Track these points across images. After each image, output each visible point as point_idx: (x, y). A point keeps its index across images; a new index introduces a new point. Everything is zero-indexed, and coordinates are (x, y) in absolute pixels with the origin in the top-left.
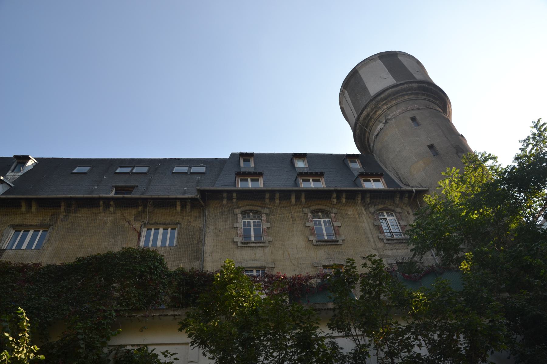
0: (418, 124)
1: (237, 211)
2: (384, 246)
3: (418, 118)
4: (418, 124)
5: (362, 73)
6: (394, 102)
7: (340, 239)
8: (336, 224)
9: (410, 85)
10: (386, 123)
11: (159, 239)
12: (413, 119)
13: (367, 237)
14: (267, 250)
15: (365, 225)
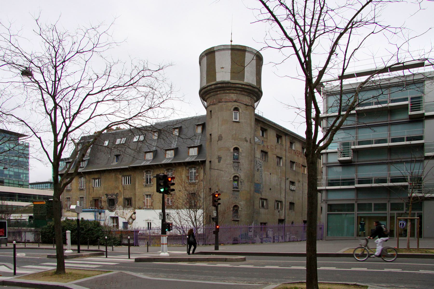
1: (144, 171)
9: (211, 87)
14: (152, 188)
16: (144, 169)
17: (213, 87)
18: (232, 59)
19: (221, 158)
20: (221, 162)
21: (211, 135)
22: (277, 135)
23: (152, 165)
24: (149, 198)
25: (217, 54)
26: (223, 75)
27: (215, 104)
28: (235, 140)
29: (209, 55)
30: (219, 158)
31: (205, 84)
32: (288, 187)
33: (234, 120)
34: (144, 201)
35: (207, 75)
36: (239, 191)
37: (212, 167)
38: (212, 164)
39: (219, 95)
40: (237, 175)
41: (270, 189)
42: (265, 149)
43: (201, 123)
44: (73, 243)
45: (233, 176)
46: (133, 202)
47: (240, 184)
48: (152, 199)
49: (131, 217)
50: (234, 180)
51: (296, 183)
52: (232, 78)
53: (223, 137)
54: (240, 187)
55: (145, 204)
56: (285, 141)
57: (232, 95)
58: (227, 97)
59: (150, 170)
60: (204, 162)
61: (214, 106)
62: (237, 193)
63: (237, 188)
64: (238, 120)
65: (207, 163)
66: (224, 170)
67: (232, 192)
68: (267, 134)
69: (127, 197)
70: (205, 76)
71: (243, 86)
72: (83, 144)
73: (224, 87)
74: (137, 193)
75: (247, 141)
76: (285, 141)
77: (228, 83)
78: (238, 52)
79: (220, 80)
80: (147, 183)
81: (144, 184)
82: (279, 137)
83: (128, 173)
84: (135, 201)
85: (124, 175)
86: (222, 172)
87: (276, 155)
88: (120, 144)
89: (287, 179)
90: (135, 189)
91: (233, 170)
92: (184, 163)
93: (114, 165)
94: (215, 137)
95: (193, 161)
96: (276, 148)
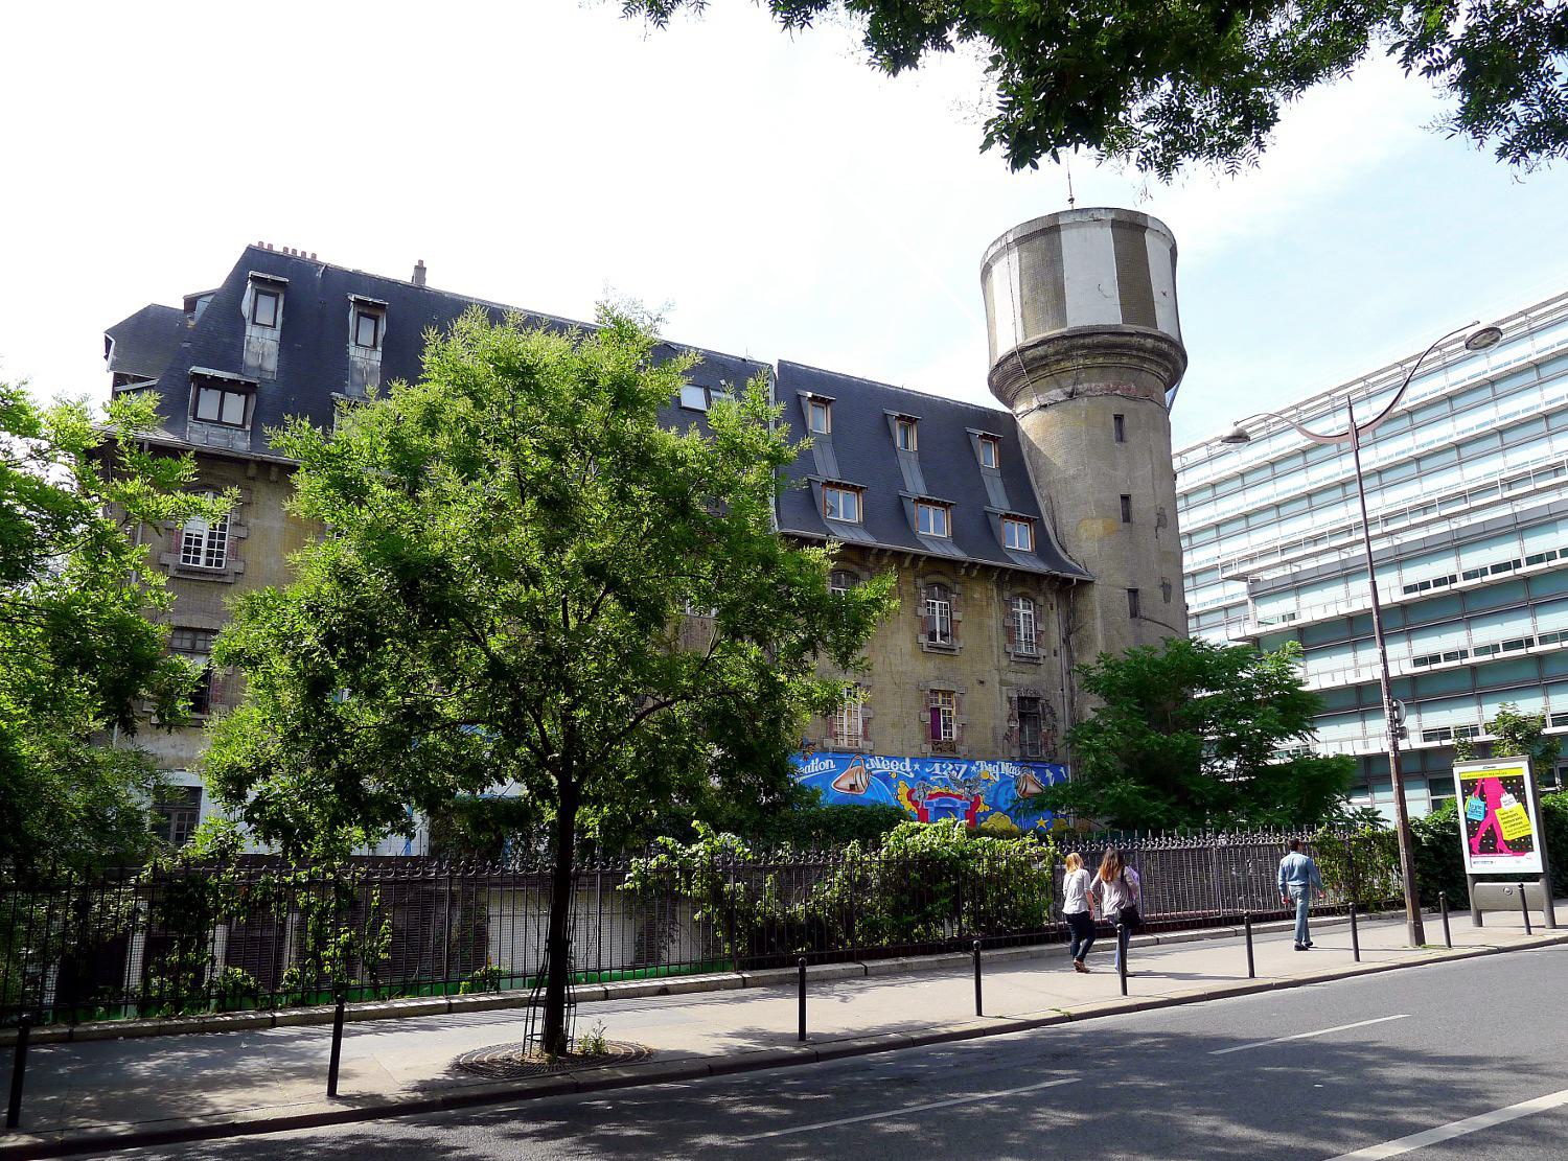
0: (1121, 438)
2: (1009, 666)
3: (1126, 420)
4: (1121, 438)
5: (1067, 238)
6: (1101, 360)
7: (957, 645)
8: (957, 616)
10: (1071, 395)
11: (694, 1100)
12: (1119, 418)
13: (991, 646)
15: (993, 622)
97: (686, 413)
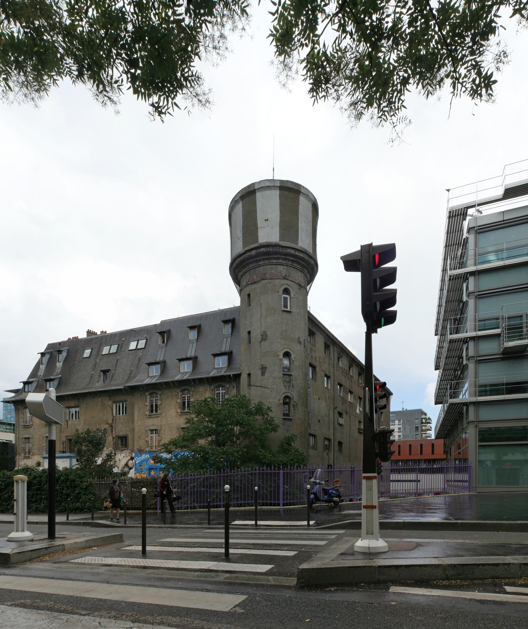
1: (147, 394)
9: (250, 253)
14: (159, 419)
16: (148, 391)
17: (253, 252)
18: (281, 204)
19: (266, 368)
20: (266, 374)
21: (249, 333)
22: (325, 343)
23: (160, 383)
24: (154, 435)
25: (258, 195)
26: (269, 233)
27: (255, 283)
28: (284, 340)
29: (247, 197)
30: (263, 369)
31: (240, 249)
32: (336, 420)
33: (283, 309)
34: (147, 439)
35: (244, 234)
36: (291, 419)
37: (252, 383)
38: (252, 378)
39: (261, 268)
40: (289, 395)
41: (319, 421)
42: (314, 362)
43: (229, 319)
44: (32, 509)
45: (283, 396)
46: (130, 442)
47: (292, 408)
48: (159, 436)
49: (127, 465)
50: (285, 403)
51: (344, 415)
52: (282, 237)
53: (269, 336)
54: (292, 413)
55: (148, 443)
56: (334, 351)
57: (281, 268)
58: (273, 271)
59: (156, 391)
60: (237, 377)
61: (254, 286)
62: (288, 423)
63: (288, 415)
64: (289, 309)
65: (244, 378)
66: (269, 387)
67: (282, 421)
68: (315, 340)
69: (121, 434)
70: (240, 234)
71: (297, 253)
72: (51, 354)
73: (270, 253)
74: (136, 428)
75: (300, 343)
76: (334, 351)
77: (276, 245)
78: (291, 193)
79: (264, 241)
80: (152, 412)
81: (147, 413)
82: (327, 347)
83: (122, 398)
84: (133, 439)
85: (116, 400)
86: (267, 390)
87: (324, 371)
88: (109, 354)
89: (336, 408)
90: (133, 422)
91: (283, 388)
92: (207, 379)
93: (99, 386)
94: (256, 335)
95: (223, 376)
96: (324, 362)
97: (147, 346)
